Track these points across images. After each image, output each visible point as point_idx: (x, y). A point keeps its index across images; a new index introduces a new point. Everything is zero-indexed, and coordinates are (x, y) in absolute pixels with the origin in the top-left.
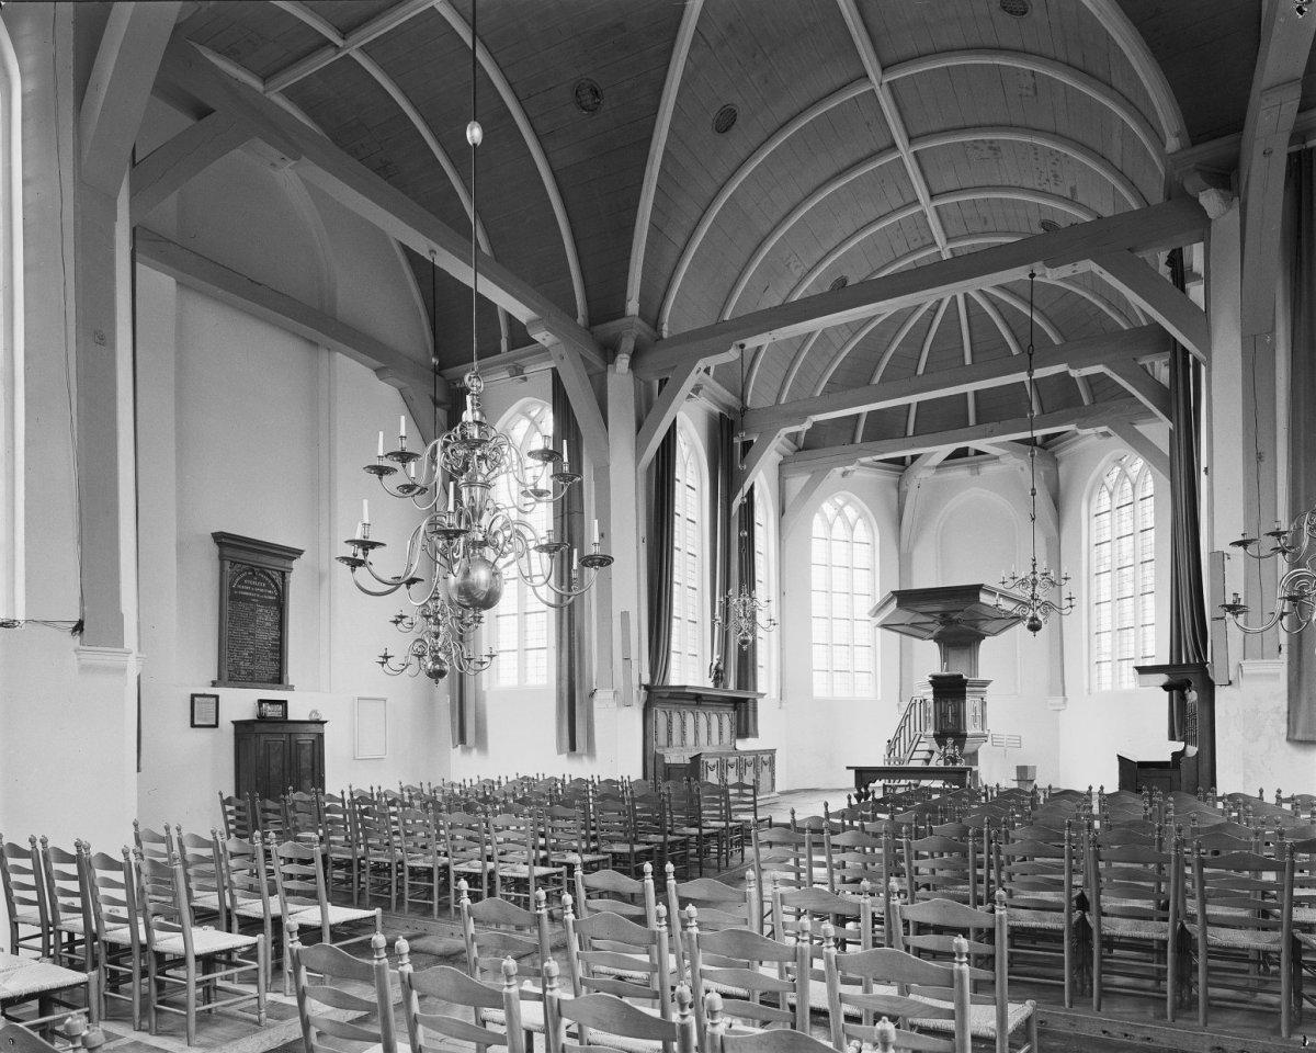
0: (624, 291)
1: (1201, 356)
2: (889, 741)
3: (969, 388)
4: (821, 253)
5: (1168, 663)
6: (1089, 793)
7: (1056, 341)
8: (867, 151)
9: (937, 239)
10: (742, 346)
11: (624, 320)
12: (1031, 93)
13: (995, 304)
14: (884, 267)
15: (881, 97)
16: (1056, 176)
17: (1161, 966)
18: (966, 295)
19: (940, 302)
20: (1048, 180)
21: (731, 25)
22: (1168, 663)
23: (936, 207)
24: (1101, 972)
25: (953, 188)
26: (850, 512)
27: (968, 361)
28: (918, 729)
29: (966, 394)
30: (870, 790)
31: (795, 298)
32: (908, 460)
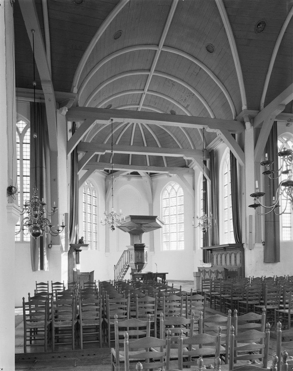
0: (72, 82)
1: (242, 164)
2: (115, 265)
3: (131, 153)
4: (111, 94)
6: (262, 278)
7: (193, 148)
8: (142, 68)
10: (112, 120)
11: (69, 94)
12: (196, 74)
13: (144, 129)
14: (122, 106)
16: (185, 100)
17: (57, 335)
19: (129, 123)
20: (182, 100)
21: (138, 4)
24: (72, 338)
25: (154, 90)
28: (219, 263)
29: (129, 154)
31: (99, 107)
32: (110, 171)
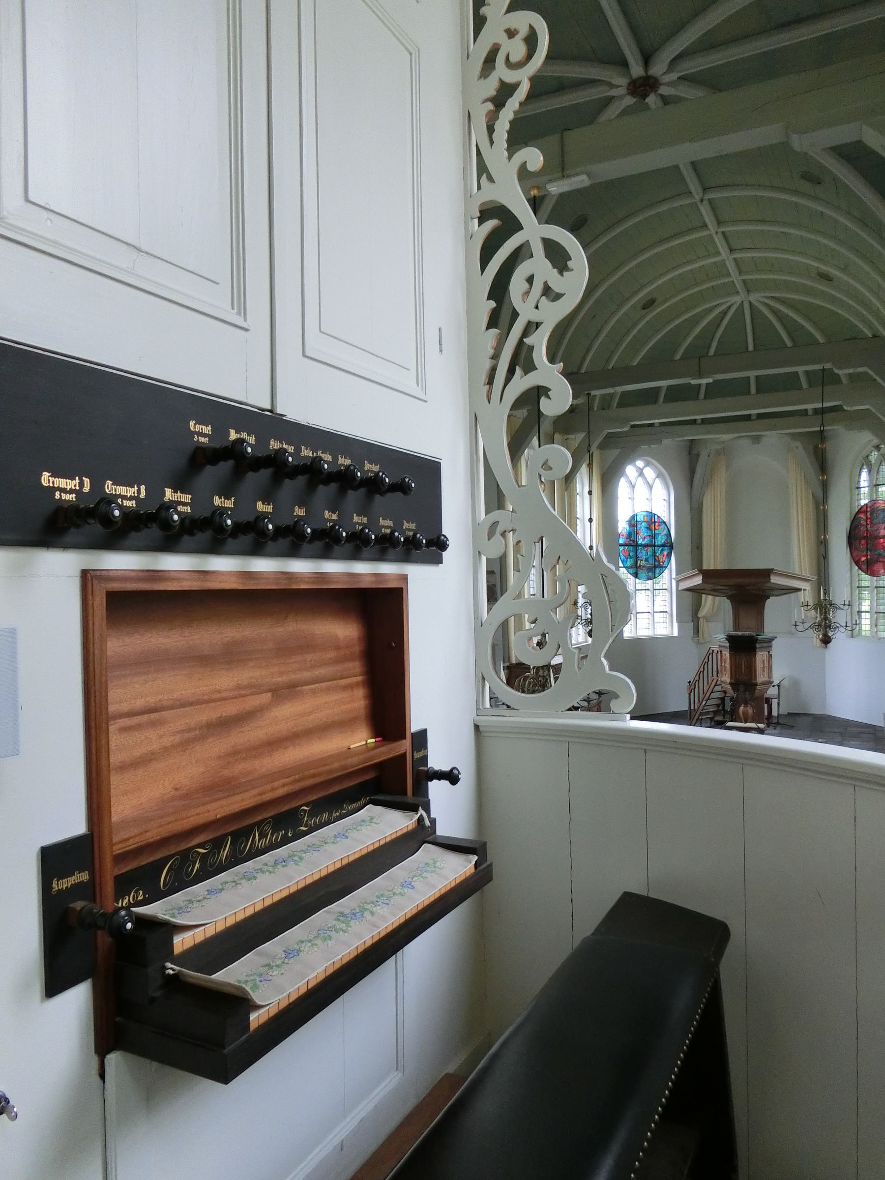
5: (687, 708)
9: (707, 221)
15: (717, 240)
18: (750, 303)
22: (687, 708)
23: (744, 281)
26: (649, 473)
27: (751, 348)
30: (315, 942)
